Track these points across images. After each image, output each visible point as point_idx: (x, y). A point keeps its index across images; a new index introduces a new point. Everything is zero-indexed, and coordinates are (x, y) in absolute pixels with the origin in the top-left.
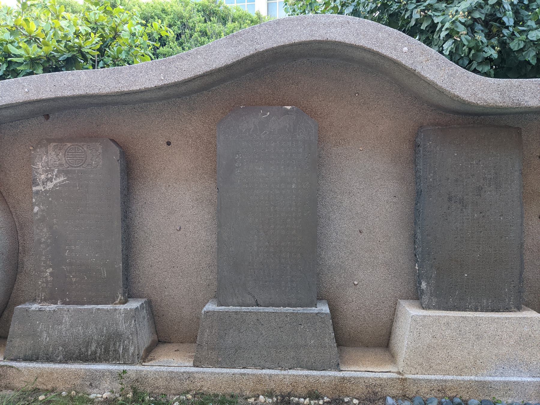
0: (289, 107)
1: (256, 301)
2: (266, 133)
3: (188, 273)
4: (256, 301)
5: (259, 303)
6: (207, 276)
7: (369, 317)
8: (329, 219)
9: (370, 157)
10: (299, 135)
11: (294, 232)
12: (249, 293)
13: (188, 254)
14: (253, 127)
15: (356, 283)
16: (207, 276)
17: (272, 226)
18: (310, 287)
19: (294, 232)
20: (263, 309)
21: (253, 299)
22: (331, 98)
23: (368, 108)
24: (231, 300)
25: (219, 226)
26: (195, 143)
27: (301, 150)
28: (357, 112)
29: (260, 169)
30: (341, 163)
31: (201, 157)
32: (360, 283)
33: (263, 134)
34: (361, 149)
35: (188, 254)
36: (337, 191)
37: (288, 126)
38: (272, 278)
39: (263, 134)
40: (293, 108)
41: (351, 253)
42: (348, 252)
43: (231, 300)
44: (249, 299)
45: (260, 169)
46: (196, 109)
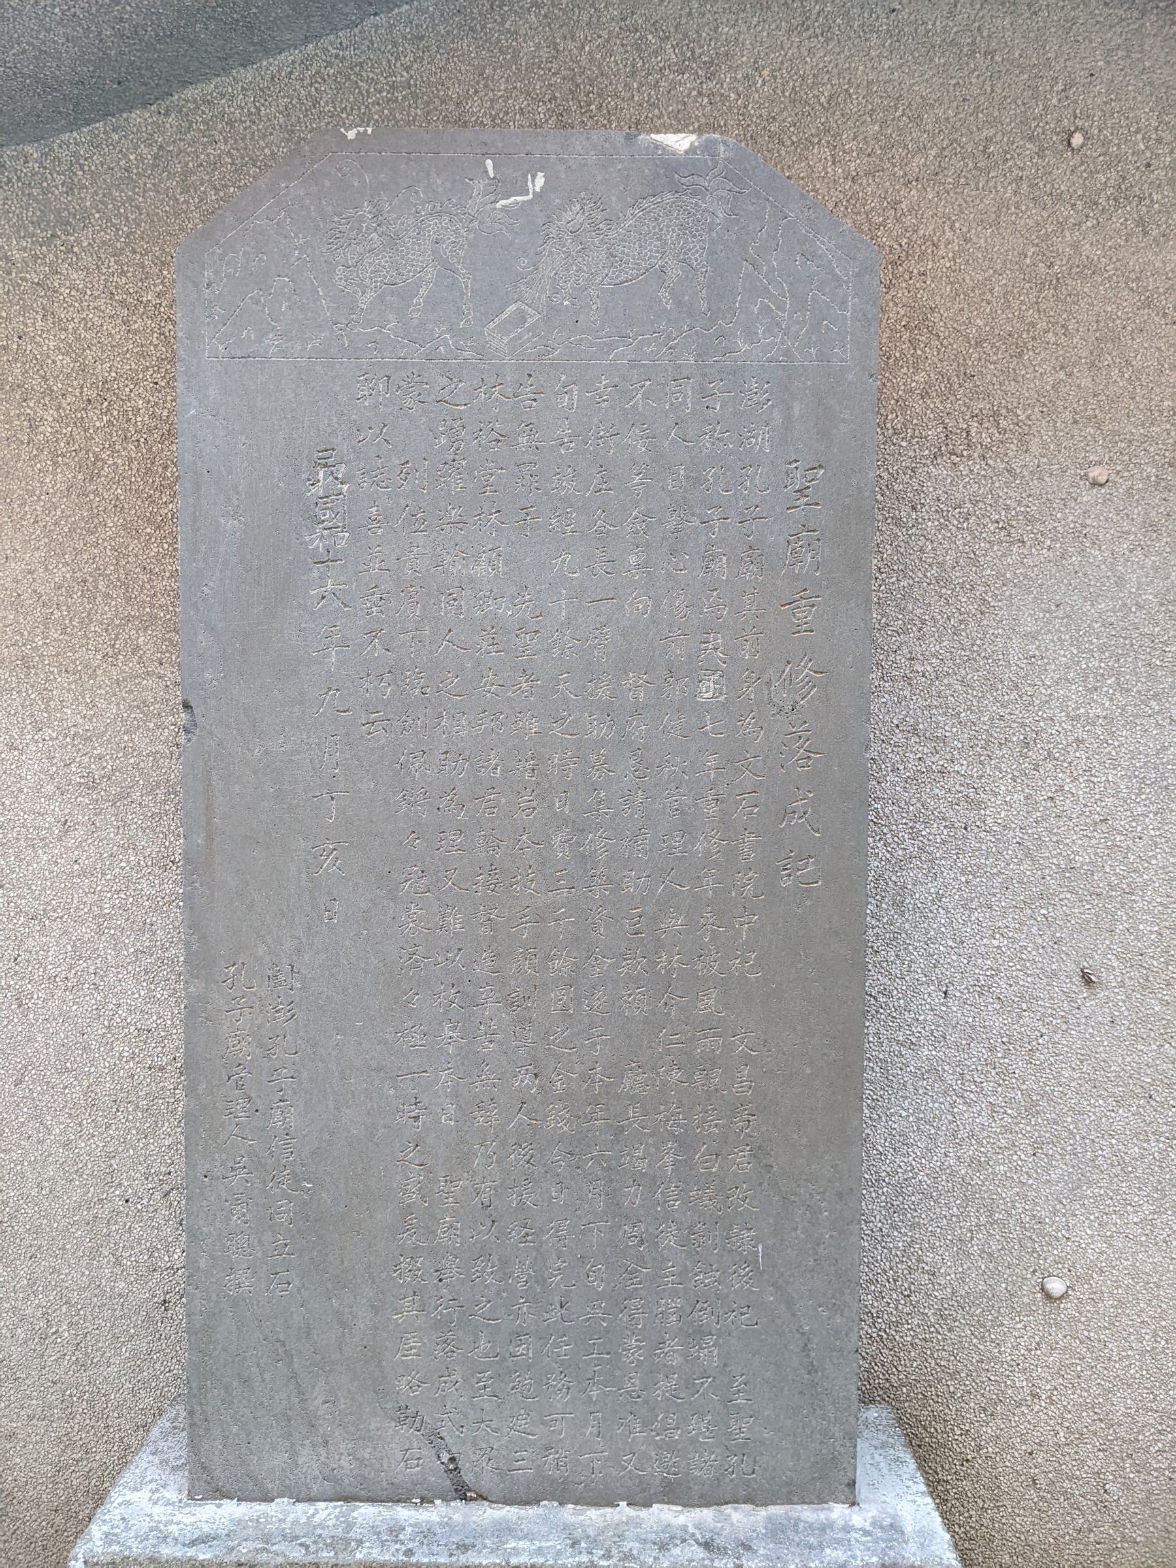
0: (680, 142)
1: (453, 1466)
2: (521, 317)
3: (37, 1231)
4: (453, 1466)
5: (468, 1478)
6: (151, 1251)
7: (1128, 1486)
8: (898, 904)
9: (1152, 527)
10: (750, 336)
11: (709, 1002)
12: (405, 1415)
13: (38, 1117)
14: (430, 274)
15: (1056, 1286)
16: (151, 1251)
17: (562, 964)
18: (812, 1370)
19: (709, 1002)
20: (504, 1530)
21: (428, 1452)
22: (919, 160)
23: (1140, 222)
24: (279, 1460)
25: (200, 963)
26: (79, 435)
27: (762, 441)
28: (1076, 246)
29: (482, 570)
30: (974, 561)
31: (113, 522)
32: (1082, 1292)
33: (503, 329)
34: (1096, 473)
35: (38, 1117)
36: (950, 730)
37: (675, 271)
38: (557, 1314)
39: (503, 329)
40: (709, 147)
41: (1031, 1110)
42: (1010, 1102)
43: (279, 1460)
44: (402, 1453)
45: (482, 570)
46: (86, 217)
